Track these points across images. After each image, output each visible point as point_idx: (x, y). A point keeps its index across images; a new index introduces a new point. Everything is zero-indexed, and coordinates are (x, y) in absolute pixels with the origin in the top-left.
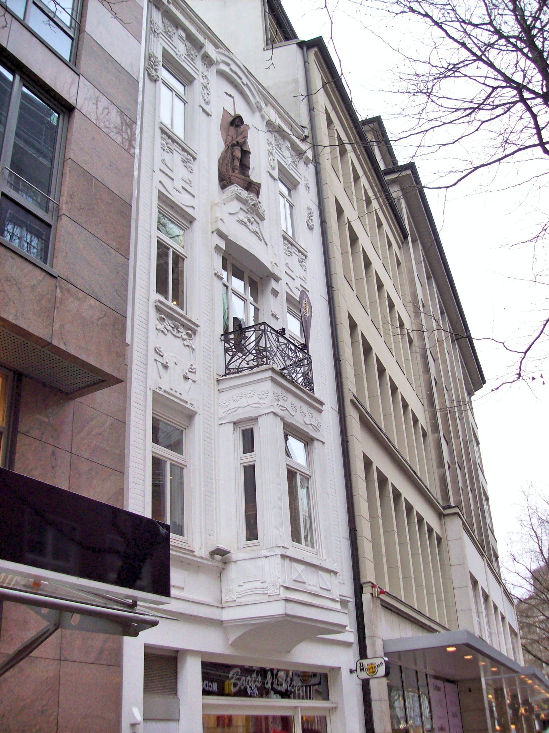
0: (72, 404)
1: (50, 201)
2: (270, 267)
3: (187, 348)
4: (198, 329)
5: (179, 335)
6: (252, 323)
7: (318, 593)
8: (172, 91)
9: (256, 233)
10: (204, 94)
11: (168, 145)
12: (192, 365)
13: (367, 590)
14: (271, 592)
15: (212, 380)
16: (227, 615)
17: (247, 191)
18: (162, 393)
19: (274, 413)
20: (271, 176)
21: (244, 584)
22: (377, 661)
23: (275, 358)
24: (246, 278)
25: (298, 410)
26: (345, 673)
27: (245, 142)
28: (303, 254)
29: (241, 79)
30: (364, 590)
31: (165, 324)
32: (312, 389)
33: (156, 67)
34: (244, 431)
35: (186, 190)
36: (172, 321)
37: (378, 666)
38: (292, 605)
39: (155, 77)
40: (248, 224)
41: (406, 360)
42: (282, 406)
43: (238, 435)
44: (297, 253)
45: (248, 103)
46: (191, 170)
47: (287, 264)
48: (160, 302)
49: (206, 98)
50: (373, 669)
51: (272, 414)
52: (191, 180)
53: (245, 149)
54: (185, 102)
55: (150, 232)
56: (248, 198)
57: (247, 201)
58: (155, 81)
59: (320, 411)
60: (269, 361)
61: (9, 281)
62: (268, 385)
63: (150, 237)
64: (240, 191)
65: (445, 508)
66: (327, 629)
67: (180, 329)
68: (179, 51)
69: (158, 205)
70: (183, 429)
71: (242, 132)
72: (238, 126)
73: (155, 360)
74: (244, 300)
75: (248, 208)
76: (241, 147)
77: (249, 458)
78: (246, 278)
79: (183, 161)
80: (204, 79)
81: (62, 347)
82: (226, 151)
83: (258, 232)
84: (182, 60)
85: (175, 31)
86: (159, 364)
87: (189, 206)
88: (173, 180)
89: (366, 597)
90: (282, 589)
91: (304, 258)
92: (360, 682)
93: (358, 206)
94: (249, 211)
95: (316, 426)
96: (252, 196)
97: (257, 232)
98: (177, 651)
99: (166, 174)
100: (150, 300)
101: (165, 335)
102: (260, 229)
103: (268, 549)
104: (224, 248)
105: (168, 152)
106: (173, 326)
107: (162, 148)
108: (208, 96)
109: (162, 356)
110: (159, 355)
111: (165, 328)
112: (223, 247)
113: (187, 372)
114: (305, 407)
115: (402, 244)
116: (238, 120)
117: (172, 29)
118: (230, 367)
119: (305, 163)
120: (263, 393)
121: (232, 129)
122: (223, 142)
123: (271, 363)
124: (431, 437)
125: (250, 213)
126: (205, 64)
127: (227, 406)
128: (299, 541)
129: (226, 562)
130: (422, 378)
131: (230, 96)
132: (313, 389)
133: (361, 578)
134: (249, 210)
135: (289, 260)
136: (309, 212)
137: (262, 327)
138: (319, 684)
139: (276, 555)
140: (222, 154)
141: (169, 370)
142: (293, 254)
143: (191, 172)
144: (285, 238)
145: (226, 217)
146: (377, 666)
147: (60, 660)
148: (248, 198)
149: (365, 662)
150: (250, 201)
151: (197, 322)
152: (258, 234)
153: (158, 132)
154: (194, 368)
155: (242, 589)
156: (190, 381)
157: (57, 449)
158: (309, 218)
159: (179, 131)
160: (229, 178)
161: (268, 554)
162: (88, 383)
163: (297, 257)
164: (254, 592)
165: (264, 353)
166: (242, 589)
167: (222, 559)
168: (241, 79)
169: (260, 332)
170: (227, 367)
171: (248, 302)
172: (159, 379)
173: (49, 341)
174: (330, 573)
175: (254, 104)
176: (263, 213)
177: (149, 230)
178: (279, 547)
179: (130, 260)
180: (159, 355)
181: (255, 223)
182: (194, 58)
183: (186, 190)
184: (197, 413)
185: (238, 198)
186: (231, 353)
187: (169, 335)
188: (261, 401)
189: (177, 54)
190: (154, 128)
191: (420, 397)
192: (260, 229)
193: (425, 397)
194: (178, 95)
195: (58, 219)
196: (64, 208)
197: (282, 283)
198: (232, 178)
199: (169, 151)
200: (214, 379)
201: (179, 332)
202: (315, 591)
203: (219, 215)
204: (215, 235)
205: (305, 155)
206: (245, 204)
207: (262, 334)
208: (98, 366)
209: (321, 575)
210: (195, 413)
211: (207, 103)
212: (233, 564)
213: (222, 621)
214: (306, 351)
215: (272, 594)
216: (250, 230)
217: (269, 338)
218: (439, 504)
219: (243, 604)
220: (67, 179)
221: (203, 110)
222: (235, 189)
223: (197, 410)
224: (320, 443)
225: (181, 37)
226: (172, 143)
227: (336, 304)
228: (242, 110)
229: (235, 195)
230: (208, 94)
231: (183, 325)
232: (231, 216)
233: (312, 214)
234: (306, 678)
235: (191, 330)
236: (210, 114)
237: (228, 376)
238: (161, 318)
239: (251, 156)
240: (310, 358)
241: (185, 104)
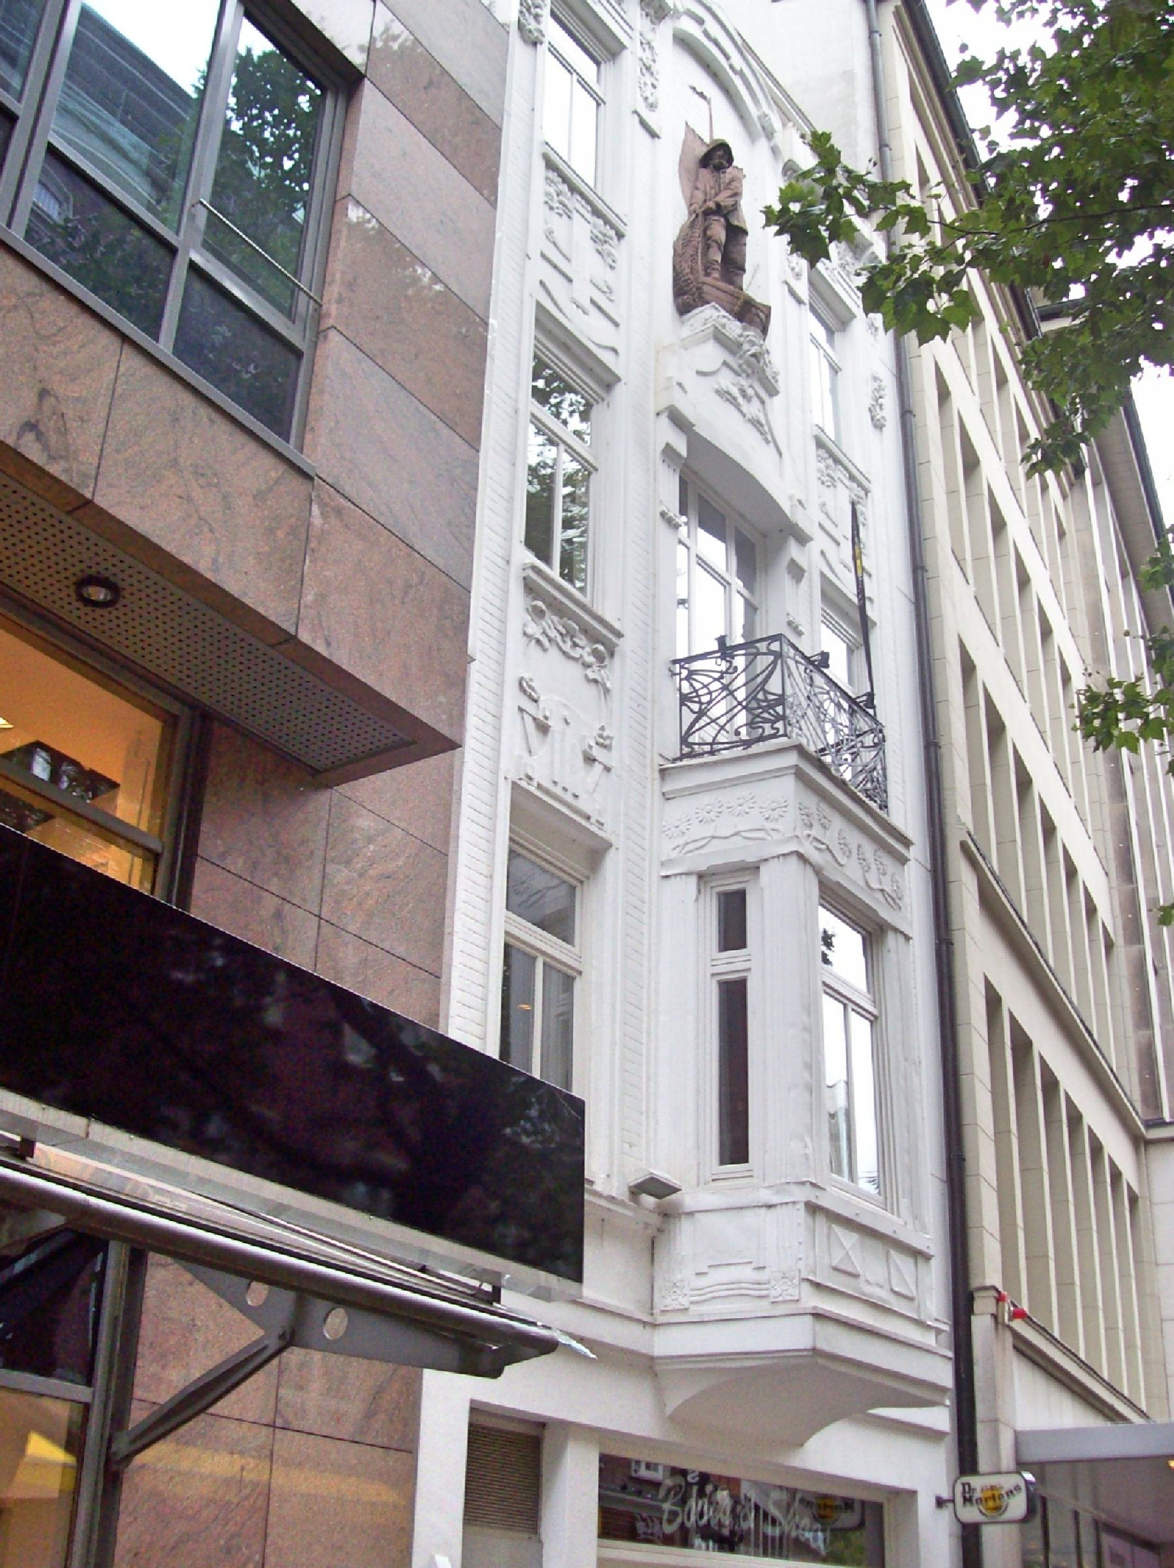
0: (323, 799)
1: (301, 293)
2: (786, 506)
3: (593, 685)
4: (621, 642)
5: (576, 653)
6: (741, 641)
9: (756, 423)
10: (645, 84)
11: (561, 198)
12: (602, 728)
13: (983, 1306)
14: (779, 1291)
15: (649, 768)
16: (666, 1344)
17: (741, 320)
18: (533, 789)
19: (801, 856)
20: (792, 293)
21: (712, 1271)
22: (1007, 1482)
23: (802, 723)
24: (730, 532)
25: (855, 852)
26: (925, 1504)
27: (735, 207)
28: (860, 485)
29: (727, 58)
30: (978, 1305)
32: (884, 806)
33: (538, 10)
34: (719, 894)
35: (600, 308)
36: (561, 618)
37: (1010, 1493)
38: (830, 1329)
39: (536, 34)
40: (740, 400)
41: (1075, 762)
42: (819, 841)
43: (708, 910)
44: (846, 481)
47: (824, 504)
48: (534, 568)
49: (648, 94)
50: (994, 1502)
51: (794, 858)
53: (736, 223)
54: (599, 102)
55: (516, 401)
56: (742, 339)
57: (740, 345)
58: (535, 44)
59: (903, 860)
60: (789, 728)
61: (202, 475)
62: (789, 784)
63: (516, 412)
65: (1149, 1125)
66: (902, 1393)
69: (536, 338)
70: (575, 883)
71: (730, 183)
72: (719, 168)
73: (521, 710)
74: (725, 584)
76: (726, 217)
77: (732, 963)
78: (730, 532)
79: (595, 239)
81: (320, 648)
82: (692, 225)
83: (764, 422)
86: (529, 721)
87: (606, 348)
88: (570, 280)
89: (981, 1324)
90: (806, 1287)
91: (862, 494)
92: (957, 1530)
93: (980, 387)
94: (744, 371)
95: (894, 896)
96: (752, 333)
97: (759, 422)
99: (555, 267)
100: (512, 563)
101: (545, 650)
103: (776, 1188)
104: (684, 453)
106: (564, 631)
109: (536, 701)
110: (530, 697)
111: (544, 633)
112: (683, 450)
113: (593, 743)
114: (869, 849)
115: (1070, 489)
116: (720, 153)
118: (695, 738)
120: (774, 805)
121: (706, 174)
122: (683, 202)
123: (794, 735)
124: (1122, 951)
125: (744, 375)
126: (647, 15)
127: (683, 833)
128: (839, 1172)
129: (669, 1215)
130: (1106, 809)
131: (701, 95)
132: (886, 807)
133: (972, 1276)
134: (744, 367)
135: (828, 495)
136: (876, 385)
137: (775, 646)
138: (861, 1525)
139: (794, 1203)
140: (681, 231)
142: (839, 484)
144: (820, 444)
145: (691, 380)
146: (1007, 1494)
147: (273, 1426)
148: (742, 339)
149: (976, 1482)
150: (746, 346)
151: (617, 625)
152: (762, 425)
153: (540, 165)
154: (608, 737)
156: (598, 768)
157: (287, 906)
159: (583, 167)
160: (699, 289)
161: (774, 1200)
162: (373, 747)
163: (847, 492)
164: (735, 1291)
165: (779, 709)
167: (659, 1206)
168: (727, 58)
169: (771, 658)
170: (684, 740)
171: (734, 589)
172: (525, 754)
173: (292, 631)
175: (756, 118)
177: (513, 395)
178: (803, 1183)
179: (481, 454)
180: (530, 697)
181: (755, 400)
183: (600, 308)
184: (610, 845)
185: (720, 338)
186: (696, 707)
187: (553, 652)
188: (769, 825)
191: (1102, 854)
192: (766, 415)
193: (1111, 854)
195: (317, 338)
196: (334, 313)
197: (814, 547)
198: (706, 288)
200: (652, 769)
201: (575, 645)
203: (674, 373)
204: (664, 420)
205: (870, 251)
206: (733, 353)
207: (774, 663)
208: (402, 704)
213: (652, 1358)
214: (871, 711)
215: (780, 1299)
216: (744, 416)
217: (790, 675)
218: (1137, 1113)
219: (706, 1319)
220: (343, 243)
221: (643, 124)
222: (710, 314)
224: (901, 939)
226: (569, 194)
227: (933, 611)
228: (728, 130)
229: (712, 329)
230: (654, 86)
231: (586, 631)
232: (701, 379)
233: (882, 393)
234: (828, 1511)
235: (603, 644)
237: (686, 762)
238: (535, 608)
239: (749, 240)
240: (881, 731)
241: (598, 105)
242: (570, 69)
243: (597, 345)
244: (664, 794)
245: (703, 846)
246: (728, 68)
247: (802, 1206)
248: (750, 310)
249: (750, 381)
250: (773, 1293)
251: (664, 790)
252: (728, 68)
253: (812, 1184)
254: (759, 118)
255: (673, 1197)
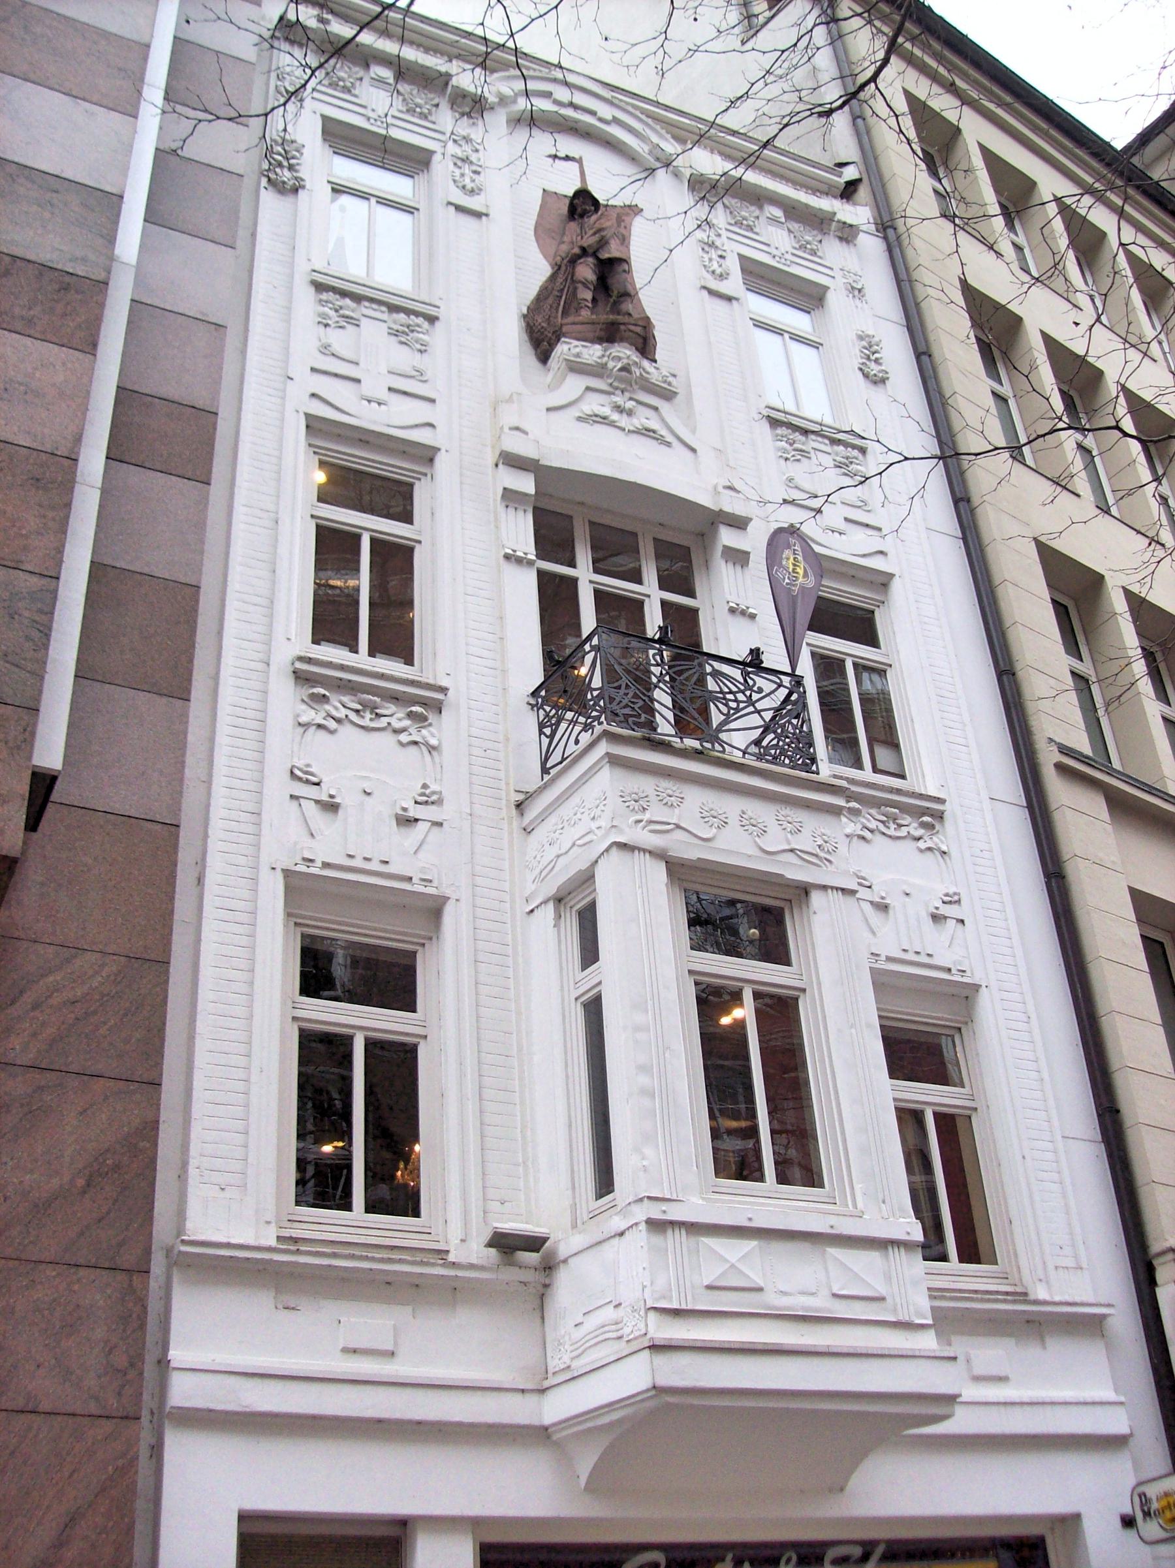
3: (929, 854)
4: (946, 807)
5: (903, 832)
7: (830, 1311)
8: (782, 335)
11: (796, 446)
12: (425, 786)
31: (864, 821)
33: (877, 355)
45: (633, 159)
46: (419, 346)
52: (864, 498)
57: (604, 366)
64: (577, 350)
67: (903, 819)
68: (373, 110)
75: (610, 381)
76: (595, 255)
79: (395, 333)
80: (460, 146)
84: (788, 263)
85: (757, 213)
94: (617, 388)
96: (624, 352)
98: (403, 1523)
99: (336, 375)
102: (663, 420)
105: (798, 460)
107: (319, 323)
108: (721, 261)
110: (307, 782)
113: (939, 904)
117: (748, 212)
119: (841, 239)
121: (573, 226)
125: (618, 392)
129: (549, 1267)
141: (891, 911)
143: (421, 351)
148: (606, 359)
150: (611, 364)
155: (583, 1330)
156: (951, 923)
158: (868, 358)
166: (583, 1330)
168: (593, 113)
174: (886, 1248)
176: (665, 382)
178: (641, 1200)
180: (307, 782)
182: (752, 223)
187: (878, 839)
189: (369, 119)
190: (290, 288)
192: (663, 420)
194: (797, 338)
199: (799, 457)
202: (803, 1308)
209: (836, 1259)
210: (976, 988)
211: (721, 275)
212: (561, 1265)
213: (546, 1428)
216: (624, 430)
223: (448, 892)
225: (773, 220)
226: (803, 438)
231: (905, 809)
236: (484, 211)
238: (313, 697)
242: (778, 331)
243: (864, 556)
244: (525, 830)
245: (553, 867)
246: (598, 124)
247: (643, 1227)
248: (618, 330)
249: (627, 395)
250: (627, 1330)
251: (524, 825)
252: (598, 124)
253: (649, 1198)
254: (650, 153)
255: (547, 1244)
